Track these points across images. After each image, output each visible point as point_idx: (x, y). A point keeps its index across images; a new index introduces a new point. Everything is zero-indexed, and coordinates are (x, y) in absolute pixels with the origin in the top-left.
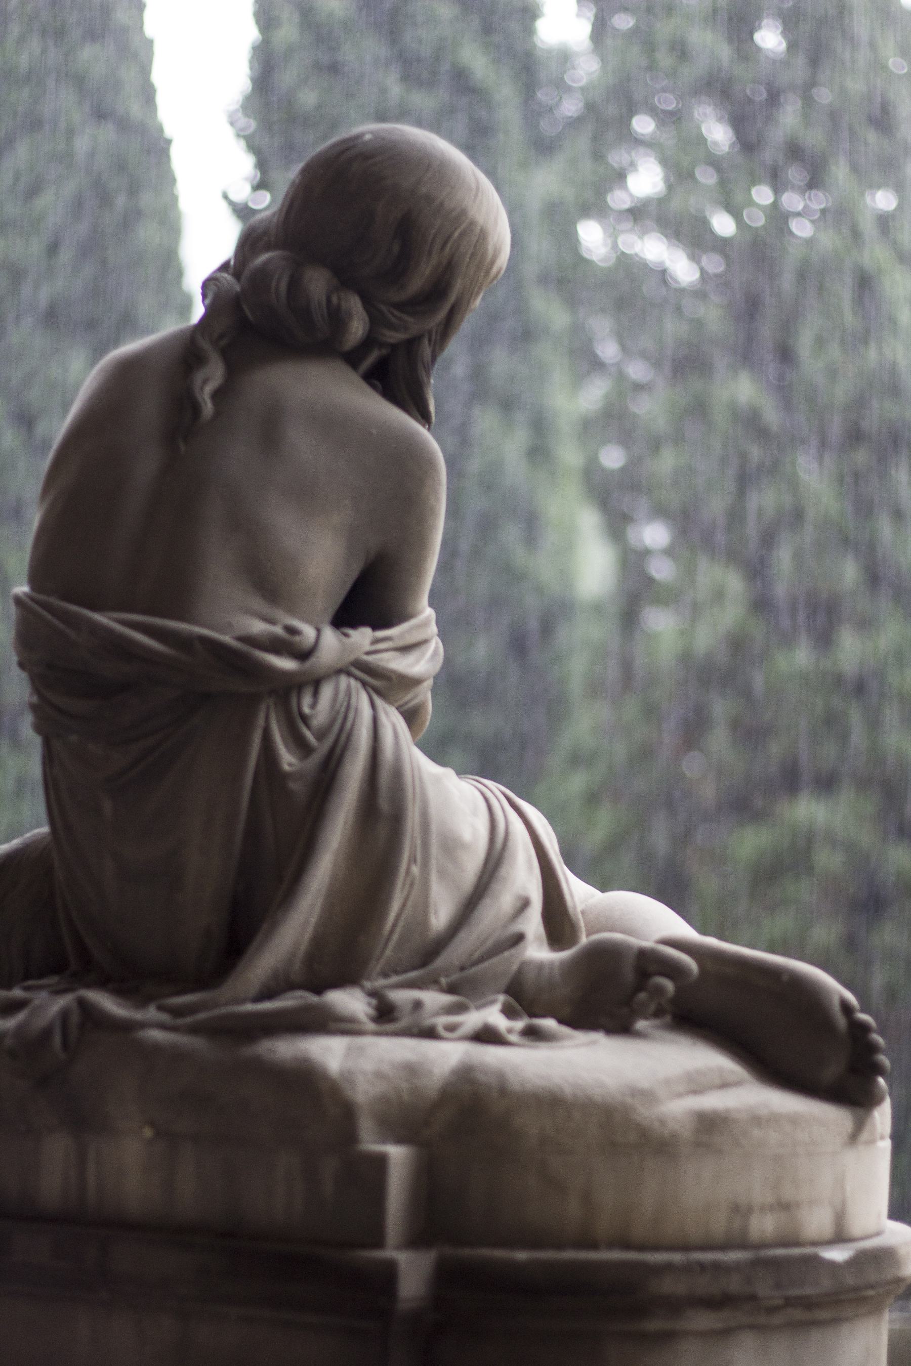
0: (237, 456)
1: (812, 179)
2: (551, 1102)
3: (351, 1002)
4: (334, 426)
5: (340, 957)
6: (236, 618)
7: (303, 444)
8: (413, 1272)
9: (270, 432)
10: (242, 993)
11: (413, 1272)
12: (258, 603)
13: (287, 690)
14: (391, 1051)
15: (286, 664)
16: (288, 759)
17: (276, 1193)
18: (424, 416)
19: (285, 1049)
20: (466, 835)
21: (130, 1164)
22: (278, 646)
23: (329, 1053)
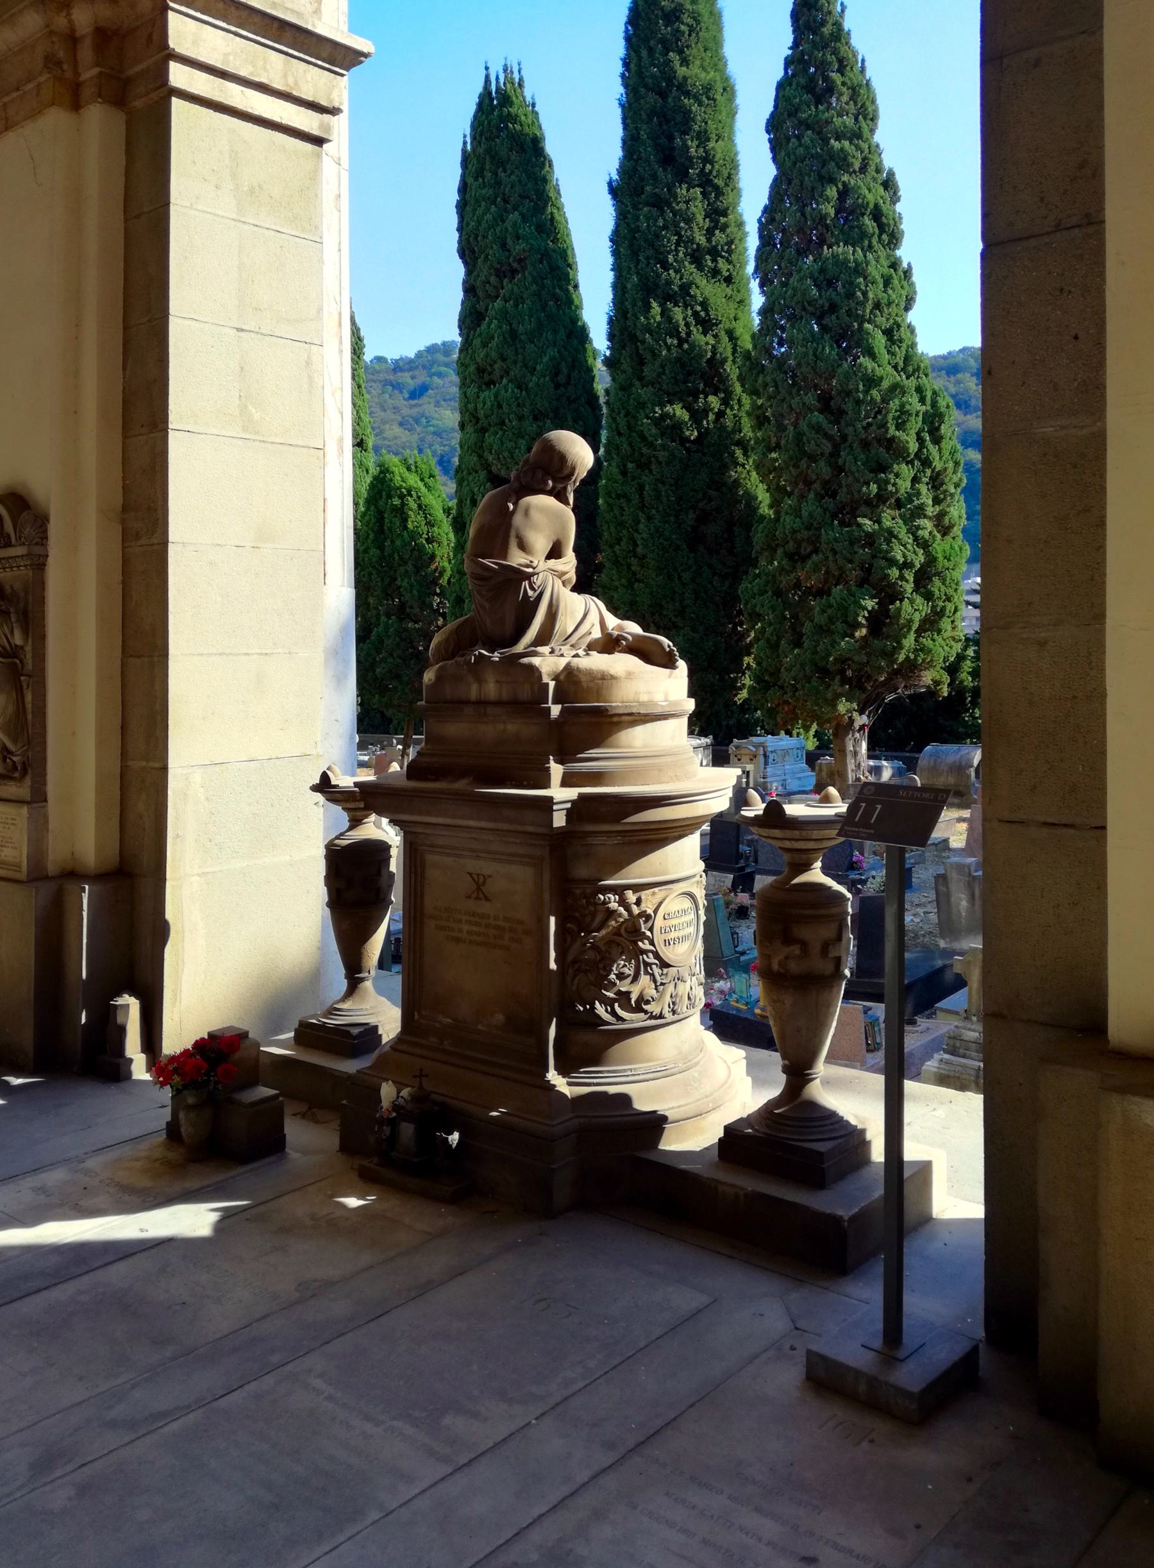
0: (518, 519)
1: (523, 703)
2: (590, 673)
3: (545, 650)
4: (545, 510)
5: (544, 638)
6: (517, 558)
7: (534, 514)
8: (555, 710)
9: (527, 513)
10: (520, 648)
11: (555, 710)
12: (523, 555)
13: (529, 577)
14: (553, 659)
15: (530, 570)
16: (530, 593)
17: (525, 693)
18: (648, 1061)
19: (525, 660)
20: (214, 1217)
21: (491, 689)
22: (528, 566)
23: (536, 661)
